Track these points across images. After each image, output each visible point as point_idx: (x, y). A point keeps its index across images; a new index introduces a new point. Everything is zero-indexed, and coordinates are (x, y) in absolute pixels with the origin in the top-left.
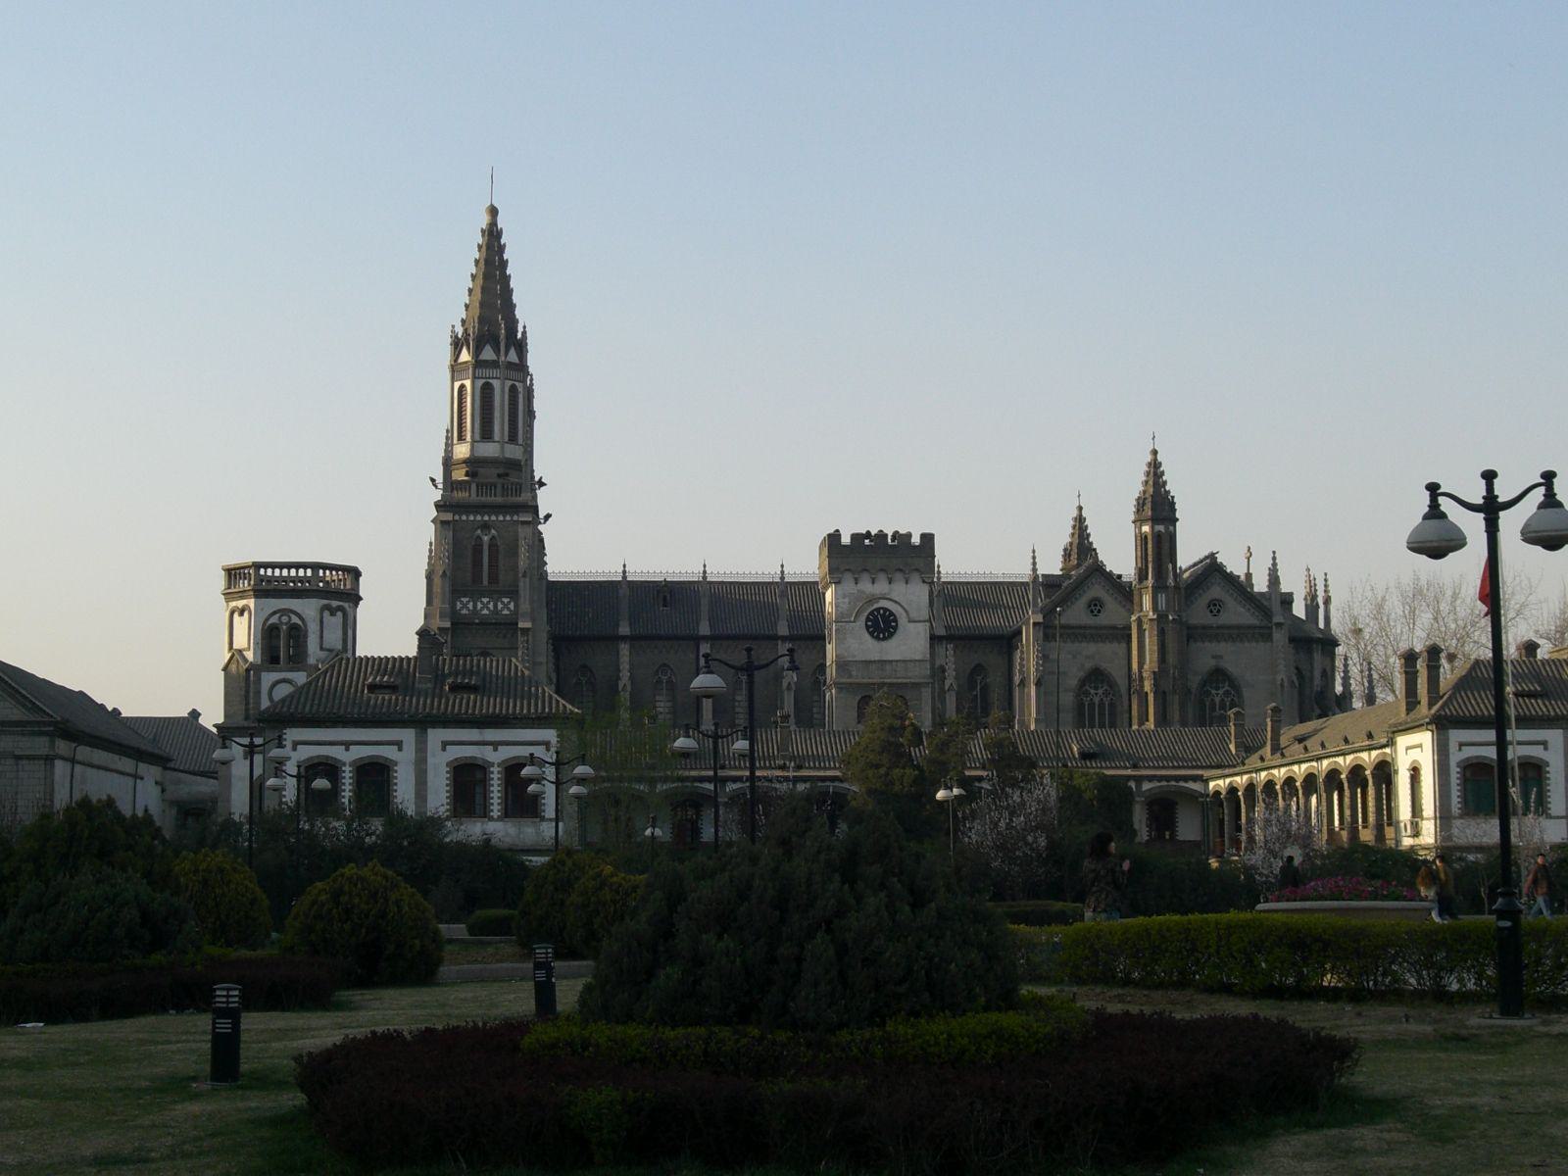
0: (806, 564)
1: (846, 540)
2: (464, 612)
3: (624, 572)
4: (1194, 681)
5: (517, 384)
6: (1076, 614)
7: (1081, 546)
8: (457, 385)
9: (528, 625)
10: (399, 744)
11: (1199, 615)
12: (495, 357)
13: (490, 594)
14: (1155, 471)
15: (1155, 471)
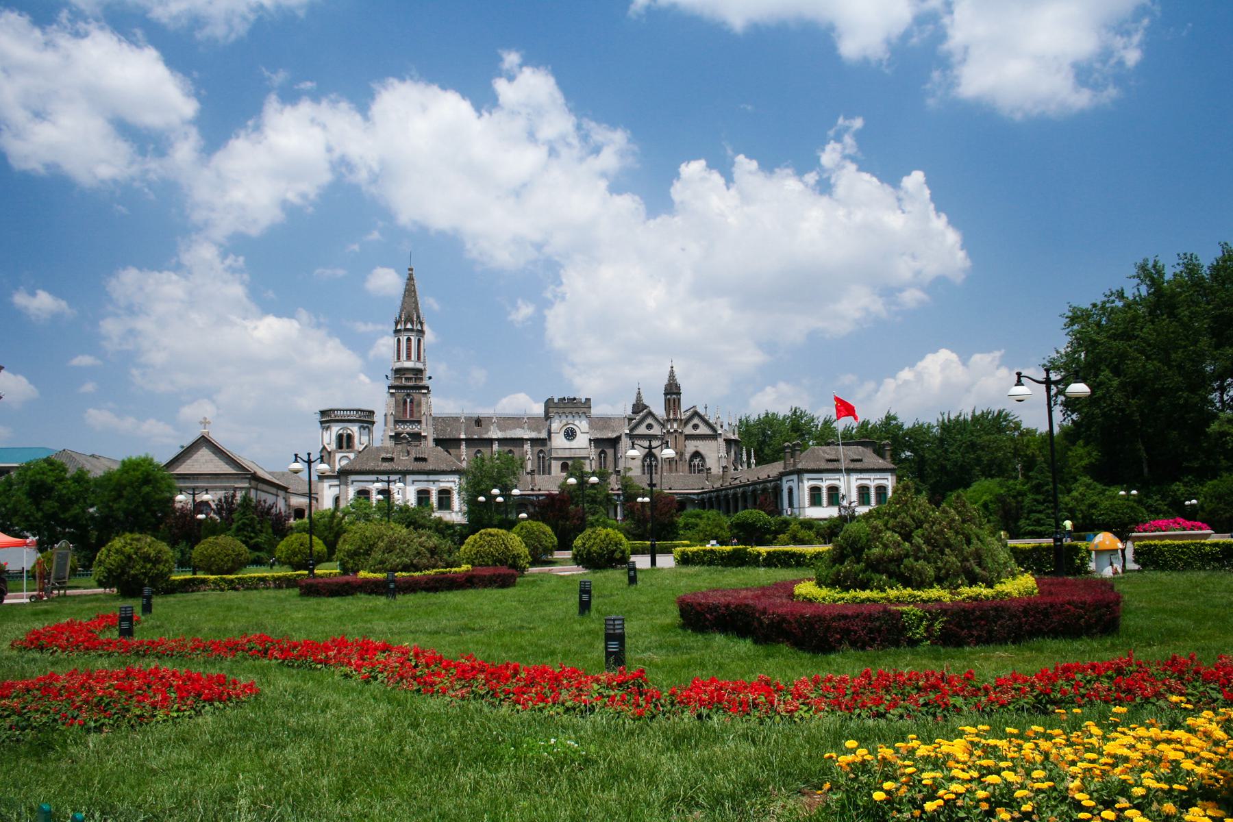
4: (687, 456)
7: (639, 407)
15: (672, 372)
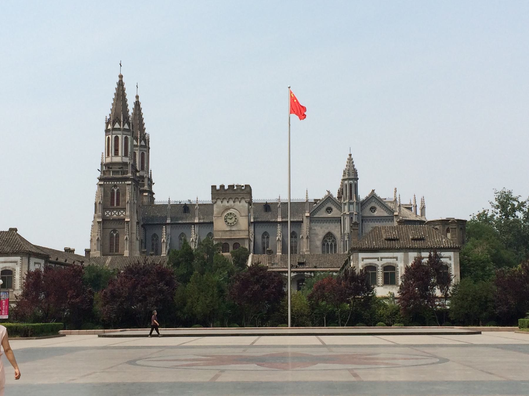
0: (206, 197)
1: (226, 187)
2: (108, 216)
3: (169, 201)
5: (118, 135)
6: (322, 214)
8: (107, 137)
9: (129, 220)
10: (450, 258)
11: (367, 213)
12: (128, 128)
13: (116, 209)
14: (350, 160)
15: (350, 160)
